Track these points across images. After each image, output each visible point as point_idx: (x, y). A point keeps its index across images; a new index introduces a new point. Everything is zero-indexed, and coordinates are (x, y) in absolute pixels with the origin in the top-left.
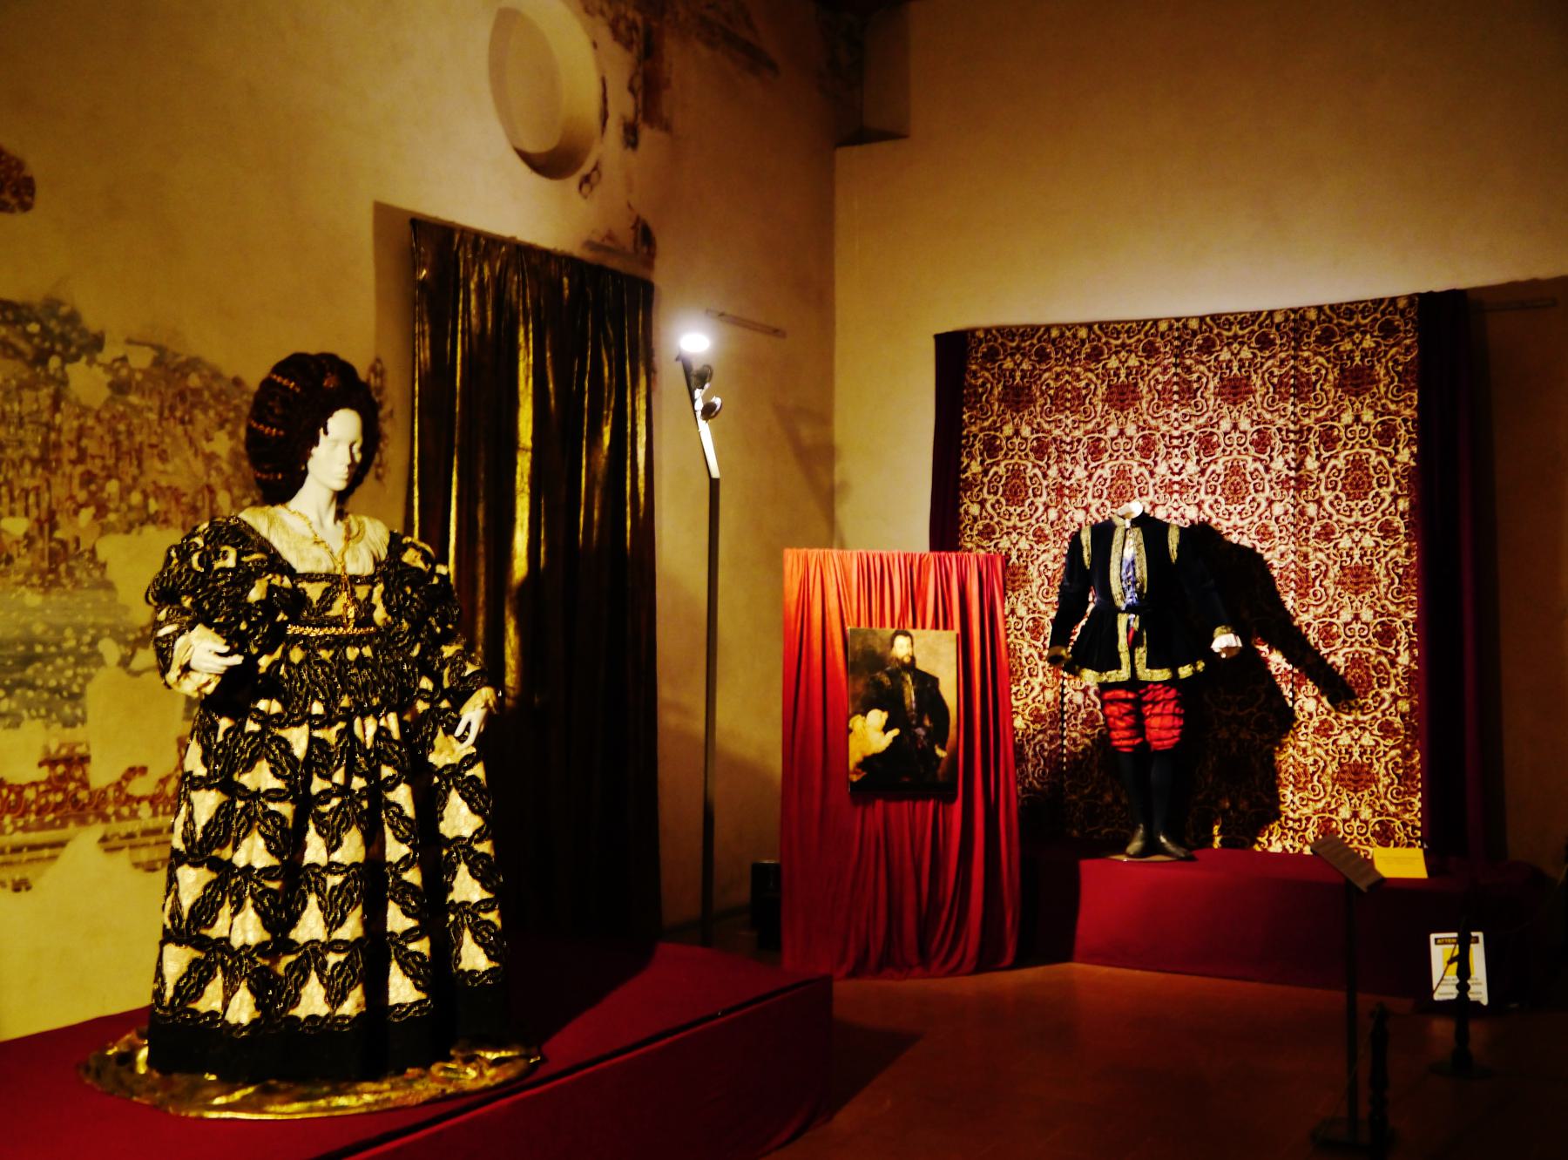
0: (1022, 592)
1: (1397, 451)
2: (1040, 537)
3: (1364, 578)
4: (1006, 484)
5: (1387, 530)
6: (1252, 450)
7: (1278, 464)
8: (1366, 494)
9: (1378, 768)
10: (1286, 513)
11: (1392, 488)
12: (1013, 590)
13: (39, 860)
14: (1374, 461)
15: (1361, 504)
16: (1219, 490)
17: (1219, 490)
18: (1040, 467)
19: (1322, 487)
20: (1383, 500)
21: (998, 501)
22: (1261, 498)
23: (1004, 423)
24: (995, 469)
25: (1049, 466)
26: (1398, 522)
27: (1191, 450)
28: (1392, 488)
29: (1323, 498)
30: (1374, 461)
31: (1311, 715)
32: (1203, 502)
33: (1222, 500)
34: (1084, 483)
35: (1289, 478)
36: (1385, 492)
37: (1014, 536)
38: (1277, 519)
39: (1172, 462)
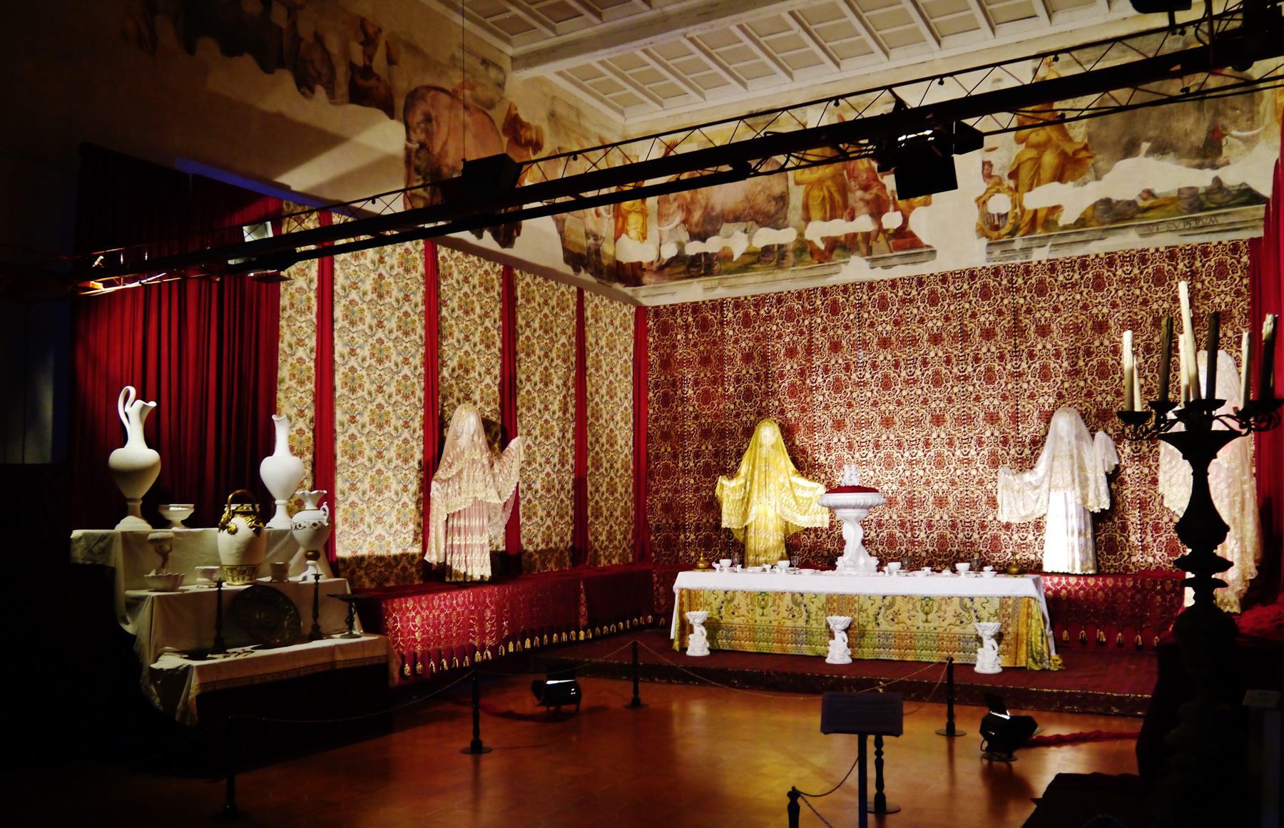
0: (840, 352)
1: (1116, 270)
2: (1114, 305)
3: (991, 333)
4: (1097, 370)
5: (1238, 293)
6: (889, 289)
7: (1181, 266)
8: (1226, 277)
9: (1001, 414)
10: (1124, 295)
11: (1239, 274)
12: (1224, 324)
13: (1073, 551)
14: (992, 284)
15: (1224, 282)
16: (1212, 274)
17: (1212, 274)
18: (1172, 265)
19: (1204, 275)
20: (1235, 280)
21: (1150, 286)
22: (894, 308)
23: (1094, 340)
24: (1087, 276)
25: (1002, 280)
26: (1243, 289)
27: (865, 290)
28: (1239, 274)
29: (1143, 287)
30: (992, 284)
31: (971, 393)
32: (1143, 287)
33: (1214, 279)
34: (916, 297)
35: (1187, 272)
36: (1236, 276)
37: (1100, 307)
38: (1120, 298)
39: (1125, 268)
